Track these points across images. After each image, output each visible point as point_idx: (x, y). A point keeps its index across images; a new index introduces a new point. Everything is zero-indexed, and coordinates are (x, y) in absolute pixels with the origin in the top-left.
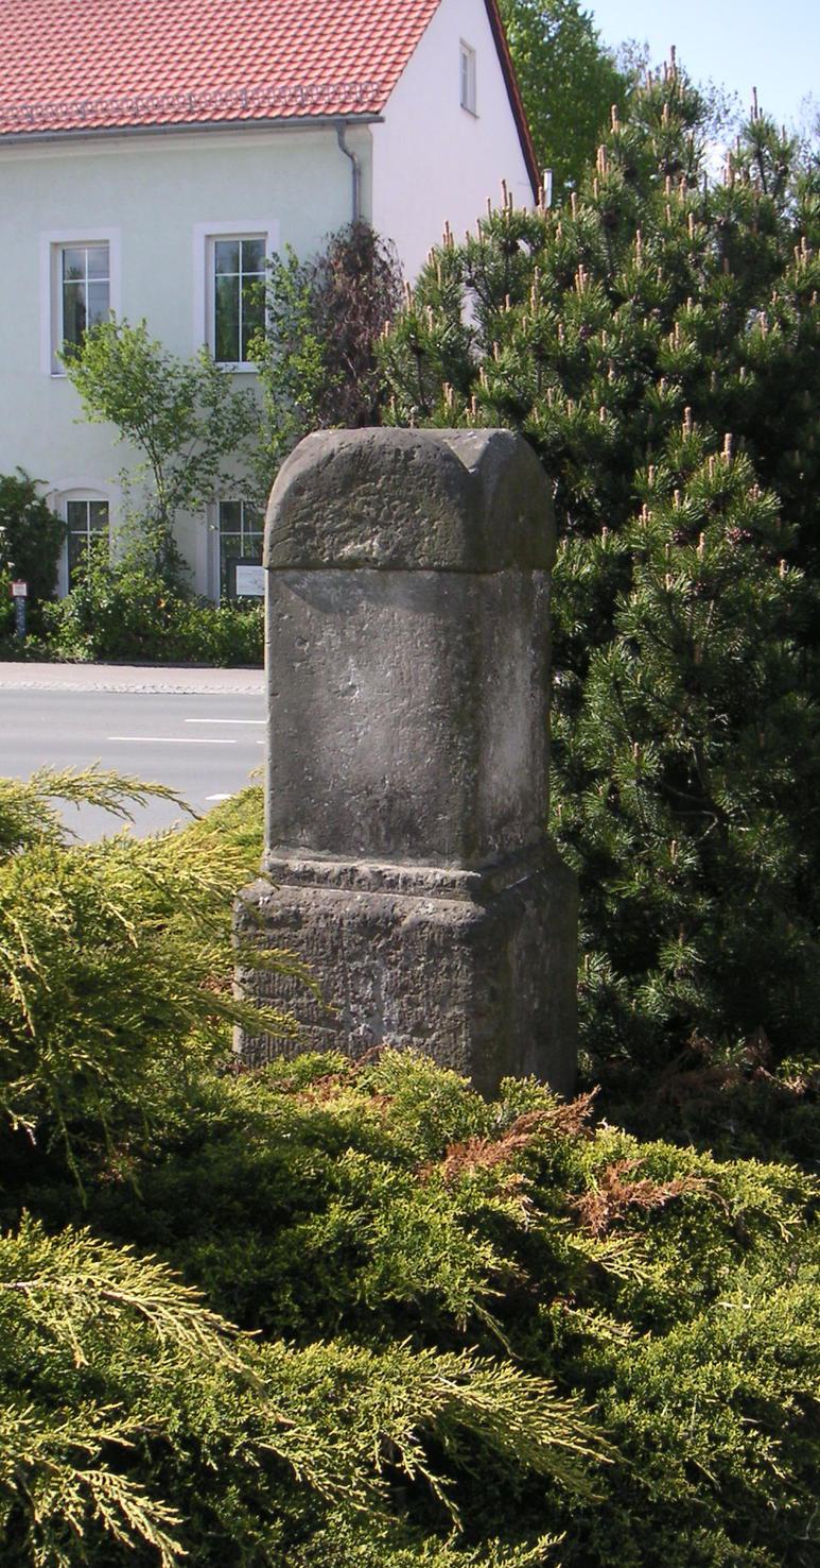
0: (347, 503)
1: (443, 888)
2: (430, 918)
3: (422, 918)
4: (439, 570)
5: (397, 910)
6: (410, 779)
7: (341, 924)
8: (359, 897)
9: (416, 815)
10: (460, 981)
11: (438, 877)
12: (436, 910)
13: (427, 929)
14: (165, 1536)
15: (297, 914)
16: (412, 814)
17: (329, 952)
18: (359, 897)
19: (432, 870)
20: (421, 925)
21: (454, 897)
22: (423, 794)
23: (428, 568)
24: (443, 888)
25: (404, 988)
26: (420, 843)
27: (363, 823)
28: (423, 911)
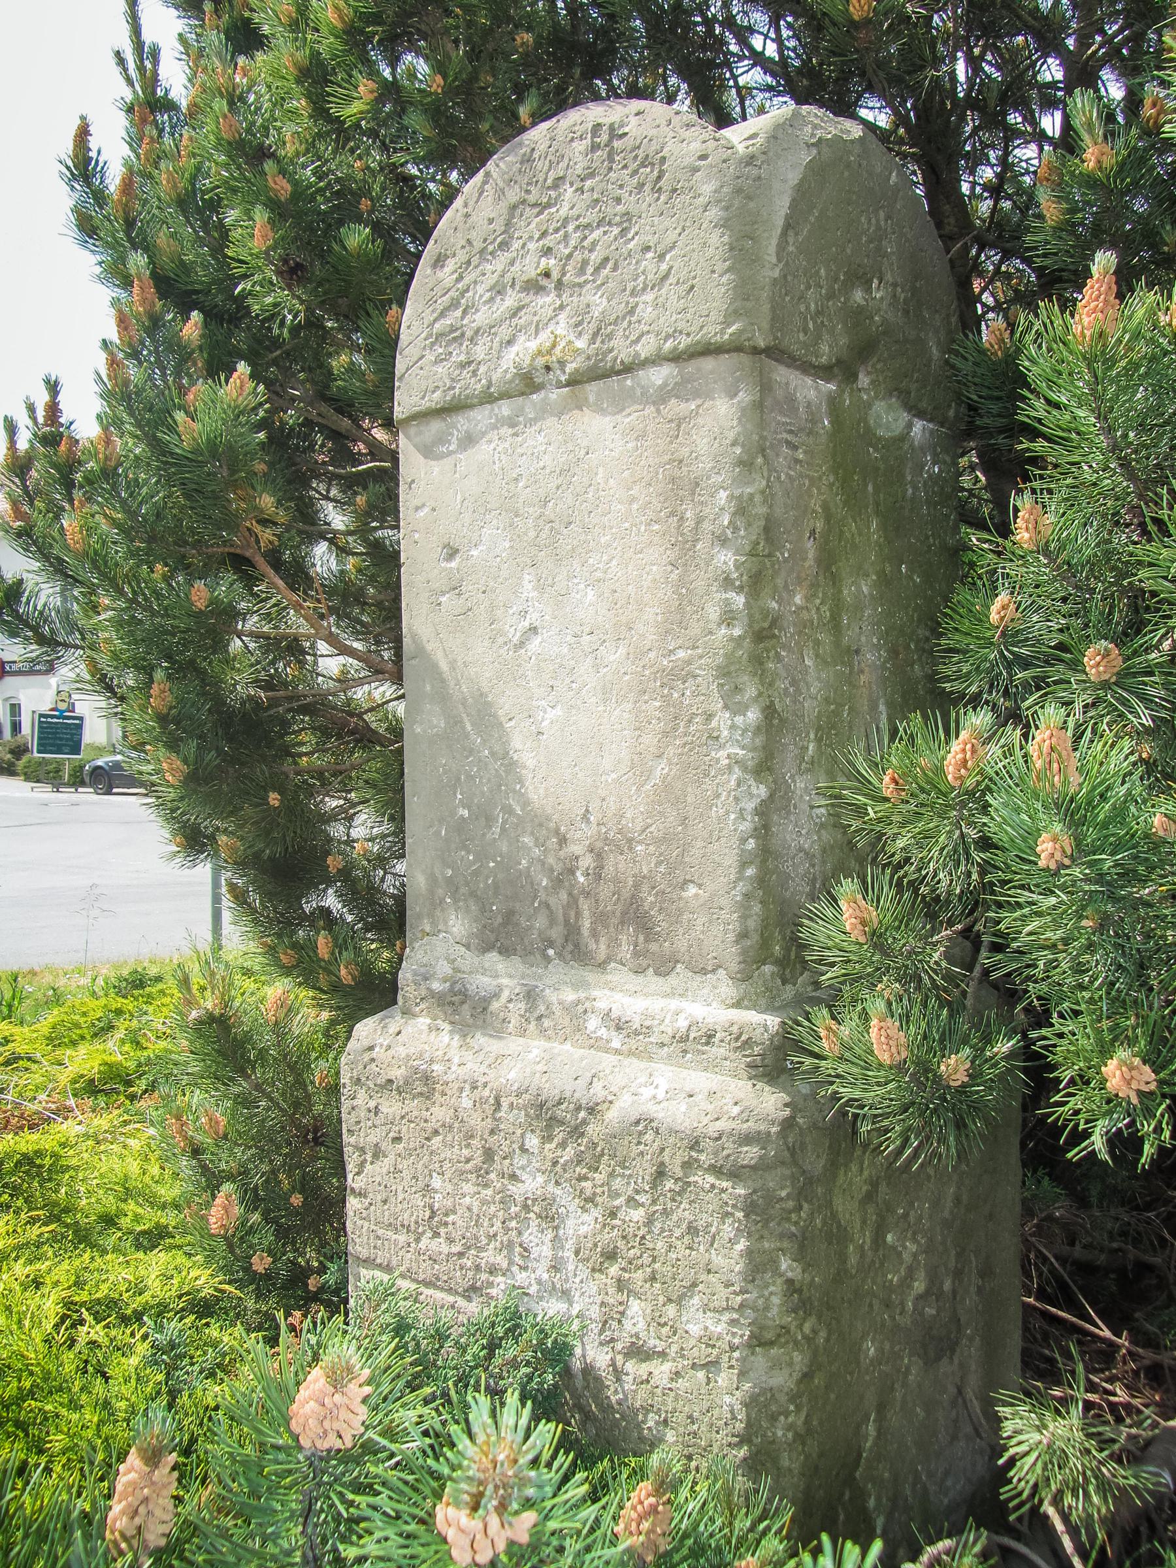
0: (512, 263)
1: (693, 1042)
2: (653, 1110)
3: (644, 1108)
4: (676, 358)
5: (597, 1086)
6: (634, 816)
7: (498, 1104)
8: (535, 1052)
9: (645, 888)
10: (718, 1260)
11: (682, 1024)
12: (670, 1095)
13: (649, 1137)
14: (1151, 1469)
15: (427, 1078)
16: (637, 886)
17: (478, 1159)
18: (535, 1052)
19: (674, 1004)
20: (642, 1124)
21: (710, 1066)
22: (658, 842)
23: (657, 359)
24: (693, 1042)
25: (611, 1255)
26: (654, 947)
27: (552, 901)
28: (647, 1092)
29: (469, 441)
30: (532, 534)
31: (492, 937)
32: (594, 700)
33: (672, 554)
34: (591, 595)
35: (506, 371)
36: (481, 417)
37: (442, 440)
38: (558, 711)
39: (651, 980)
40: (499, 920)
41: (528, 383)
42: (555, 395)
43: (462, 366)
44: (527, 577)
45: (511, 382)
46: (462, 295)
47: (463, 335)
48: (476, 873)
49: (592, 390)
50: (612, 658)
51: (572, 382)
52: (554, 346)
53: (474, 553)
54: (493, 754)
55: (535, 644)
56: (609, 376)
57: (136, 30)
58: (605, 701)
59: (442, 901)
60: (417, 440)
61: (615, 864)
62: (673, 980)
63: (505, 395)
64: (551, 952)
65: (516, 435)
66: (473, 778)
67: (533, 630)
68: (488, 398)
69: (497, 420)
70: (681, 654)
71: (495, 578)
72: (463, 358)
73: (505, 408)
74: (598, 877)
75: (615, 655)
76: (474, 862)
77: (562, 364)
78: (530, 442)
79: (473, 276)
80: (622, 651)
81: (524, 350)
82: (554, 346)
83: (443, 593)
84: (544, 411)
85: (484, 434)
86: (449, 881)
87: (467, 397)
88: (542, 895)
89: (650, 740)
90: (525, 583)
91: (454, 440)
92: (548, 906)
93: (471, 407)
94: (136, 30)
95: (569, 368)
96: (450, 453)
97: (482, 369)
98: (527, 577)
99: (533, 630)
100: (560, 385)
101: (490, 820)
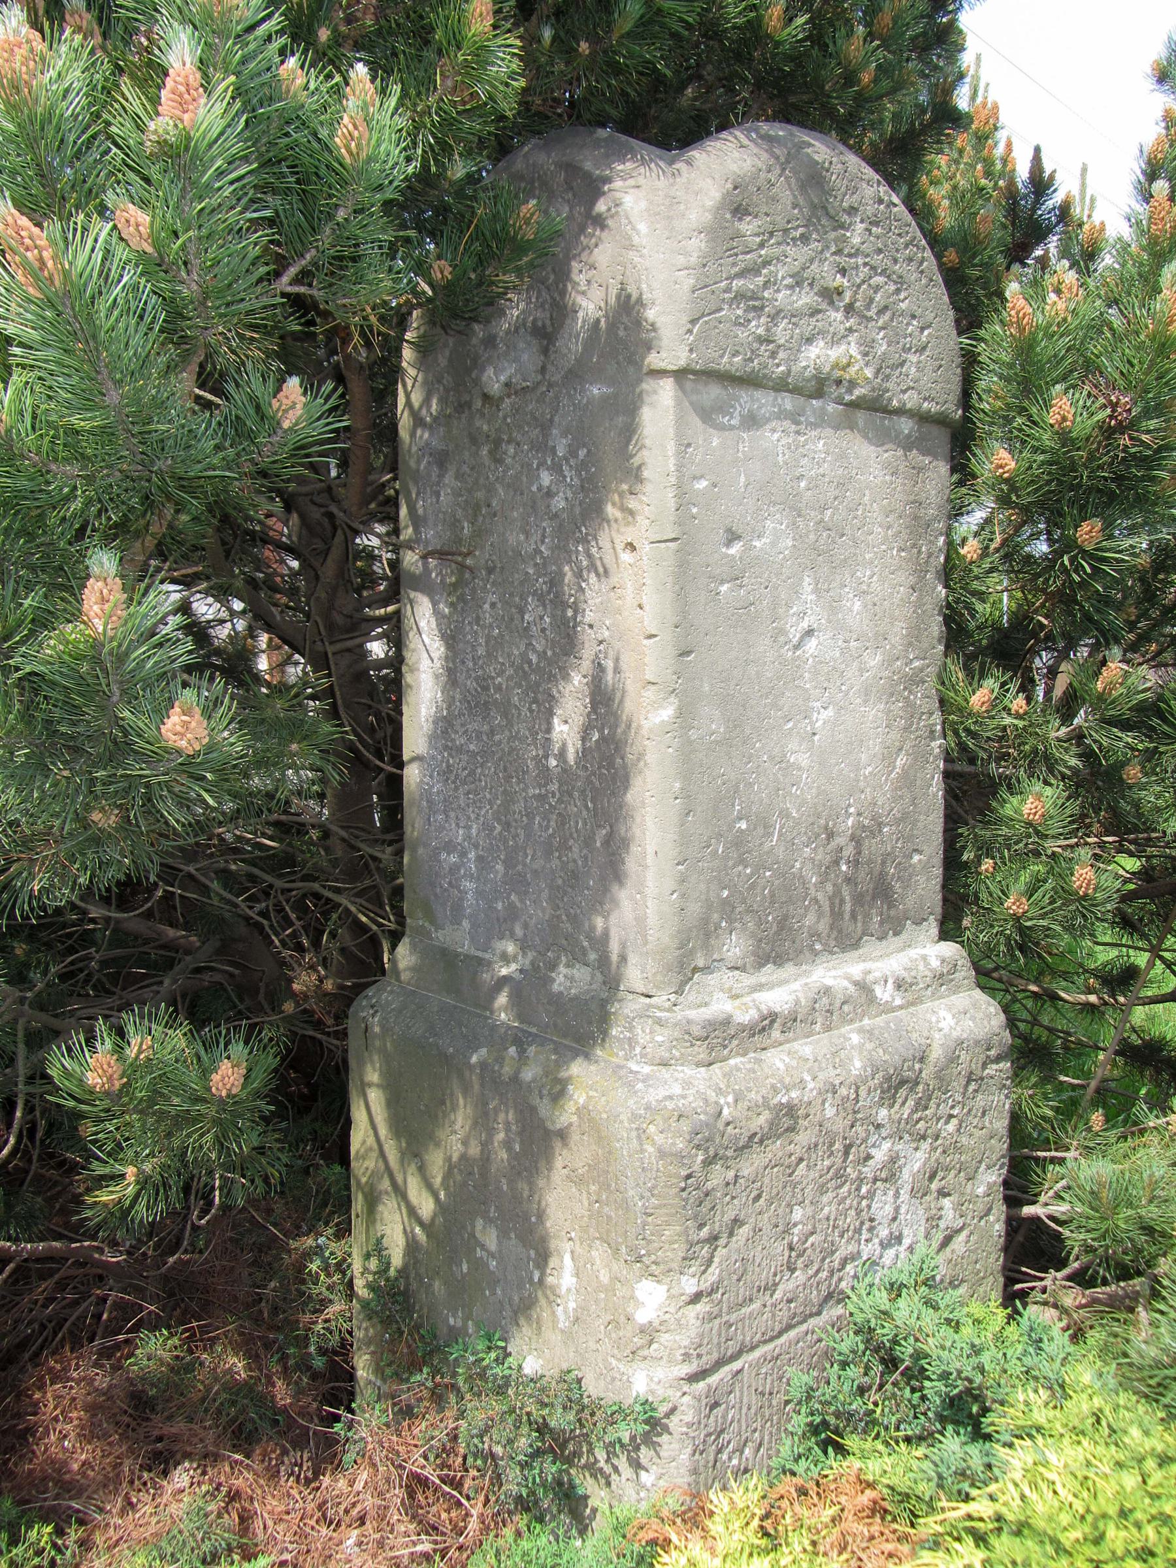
22: (898, 822)
29: (752, 421)
30: (812, 537)
31: (768, 948)
32: (858, 701)
33: (912, 580)
34: (857, 606)
35: (805, 368)
36: (763, 401)
37: (722, 408)
38: (830, 712)
39: (893, 942)
40: (775, 928)
41: (819, 386)
42: (831, 407)
43: (761, 340)
44: (807, 579)
45: (808, 381)
46: (766, 263)
47: (762, 308)
48: (753, 887)
49: (861, 417)
50: (872, 663)
51: (854, 405)
52: (848, 365)
53: (757, 544)
54: (772, 758)
55: (812, 645)
56: (876, 410)
57: (1083, 185)
58: (866, 701)
59: (718, 927)
60: (694, 398)
61: (871, 846)
62: (904, 936)
63: (796, 391)
64: (818, 947)
65: (798, 433)
66: (751, 785)
67: (809, 632)
68: (781, 386)
69: (780, 412)
70: (917, 664)
71: (777, 575)
72: (761, 331)
73: (788, 402)
74: (857, 863)
75: (874, 661)
76: (752, 874)
77: (852, 384)
78: (810, 446)
79: (777, 251)
80: (879, 658)
81: (817, 355)
82: (848, 365)
83: (722, 582)
84: (821, 421)
85: (768, 420)
86: (725, 902)
87: (765, 376)
88: (812, 891)
89: (895, 735)
90: (805, 584)
91: (736, 414)
92: (817, 901)
93: (764, 387)
94: (1083, 185)
95: (857, 392)
96: (732, 428)
97: (782, 355)
98: (807, 579)
99: (809, 632)
100: (839, 401)
101: (768, 828)
